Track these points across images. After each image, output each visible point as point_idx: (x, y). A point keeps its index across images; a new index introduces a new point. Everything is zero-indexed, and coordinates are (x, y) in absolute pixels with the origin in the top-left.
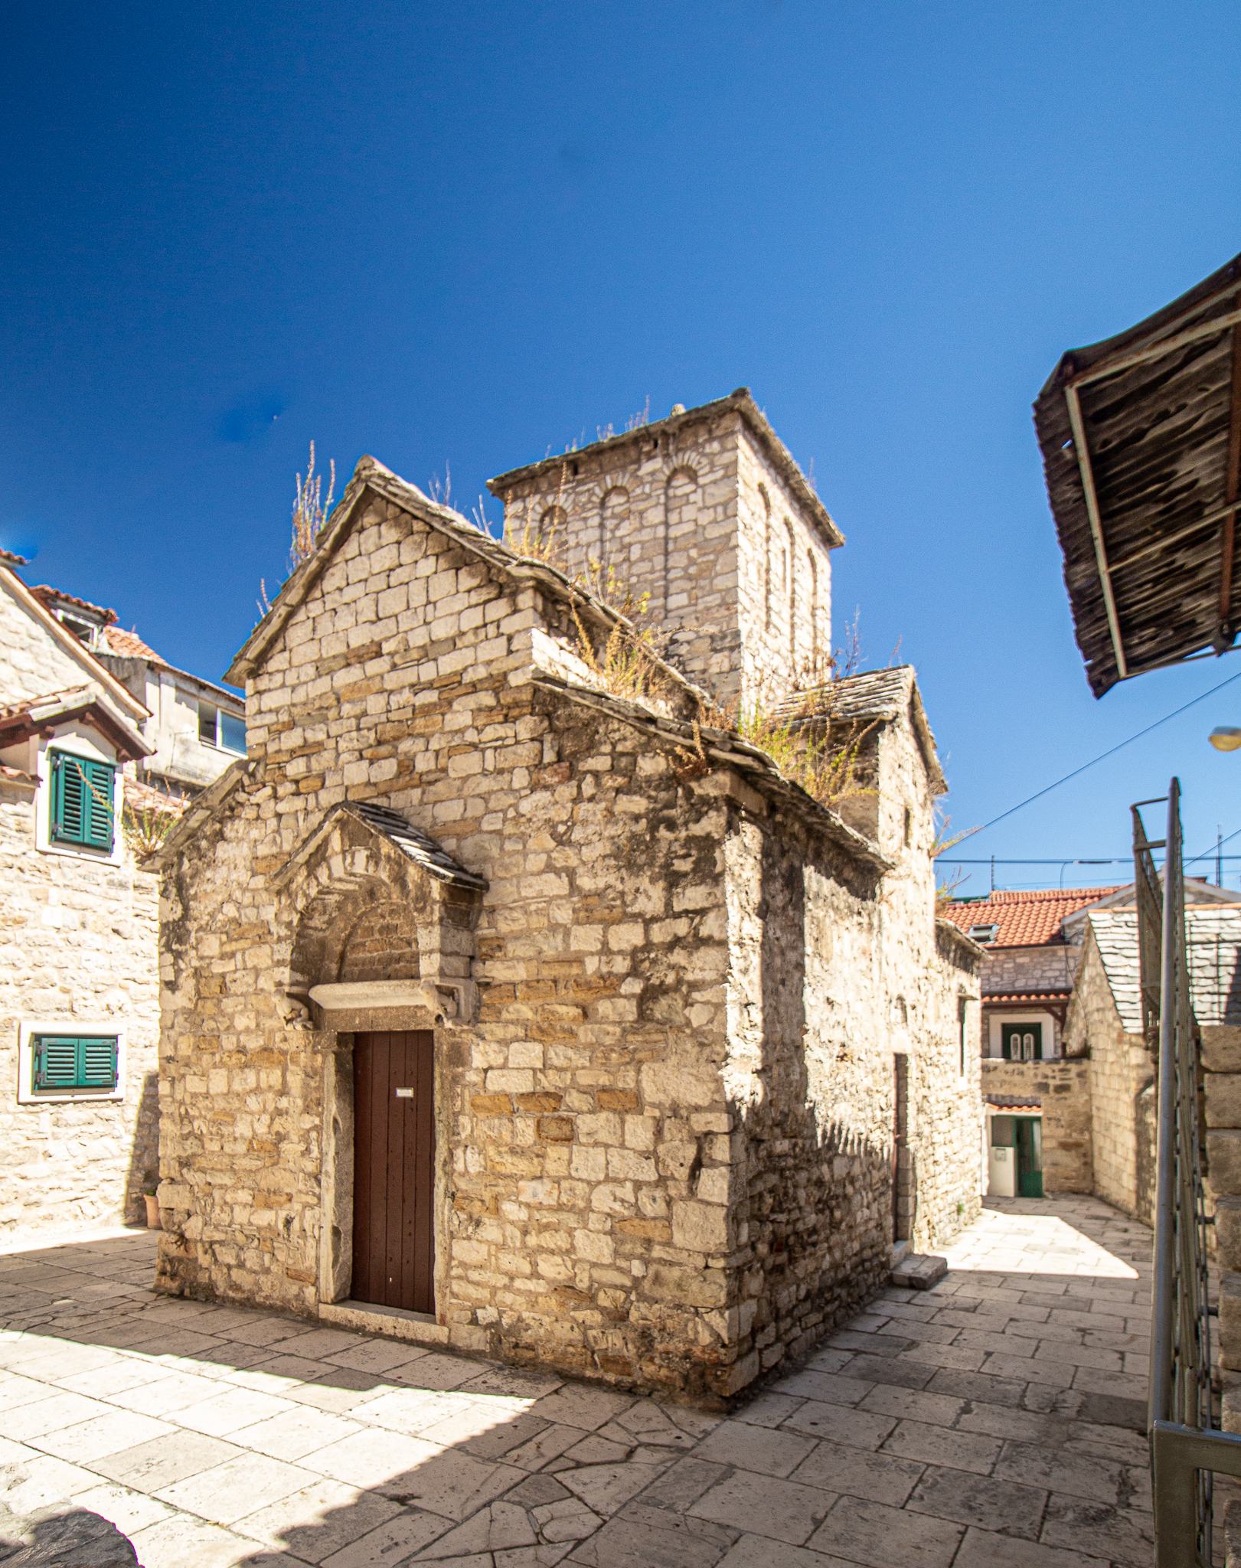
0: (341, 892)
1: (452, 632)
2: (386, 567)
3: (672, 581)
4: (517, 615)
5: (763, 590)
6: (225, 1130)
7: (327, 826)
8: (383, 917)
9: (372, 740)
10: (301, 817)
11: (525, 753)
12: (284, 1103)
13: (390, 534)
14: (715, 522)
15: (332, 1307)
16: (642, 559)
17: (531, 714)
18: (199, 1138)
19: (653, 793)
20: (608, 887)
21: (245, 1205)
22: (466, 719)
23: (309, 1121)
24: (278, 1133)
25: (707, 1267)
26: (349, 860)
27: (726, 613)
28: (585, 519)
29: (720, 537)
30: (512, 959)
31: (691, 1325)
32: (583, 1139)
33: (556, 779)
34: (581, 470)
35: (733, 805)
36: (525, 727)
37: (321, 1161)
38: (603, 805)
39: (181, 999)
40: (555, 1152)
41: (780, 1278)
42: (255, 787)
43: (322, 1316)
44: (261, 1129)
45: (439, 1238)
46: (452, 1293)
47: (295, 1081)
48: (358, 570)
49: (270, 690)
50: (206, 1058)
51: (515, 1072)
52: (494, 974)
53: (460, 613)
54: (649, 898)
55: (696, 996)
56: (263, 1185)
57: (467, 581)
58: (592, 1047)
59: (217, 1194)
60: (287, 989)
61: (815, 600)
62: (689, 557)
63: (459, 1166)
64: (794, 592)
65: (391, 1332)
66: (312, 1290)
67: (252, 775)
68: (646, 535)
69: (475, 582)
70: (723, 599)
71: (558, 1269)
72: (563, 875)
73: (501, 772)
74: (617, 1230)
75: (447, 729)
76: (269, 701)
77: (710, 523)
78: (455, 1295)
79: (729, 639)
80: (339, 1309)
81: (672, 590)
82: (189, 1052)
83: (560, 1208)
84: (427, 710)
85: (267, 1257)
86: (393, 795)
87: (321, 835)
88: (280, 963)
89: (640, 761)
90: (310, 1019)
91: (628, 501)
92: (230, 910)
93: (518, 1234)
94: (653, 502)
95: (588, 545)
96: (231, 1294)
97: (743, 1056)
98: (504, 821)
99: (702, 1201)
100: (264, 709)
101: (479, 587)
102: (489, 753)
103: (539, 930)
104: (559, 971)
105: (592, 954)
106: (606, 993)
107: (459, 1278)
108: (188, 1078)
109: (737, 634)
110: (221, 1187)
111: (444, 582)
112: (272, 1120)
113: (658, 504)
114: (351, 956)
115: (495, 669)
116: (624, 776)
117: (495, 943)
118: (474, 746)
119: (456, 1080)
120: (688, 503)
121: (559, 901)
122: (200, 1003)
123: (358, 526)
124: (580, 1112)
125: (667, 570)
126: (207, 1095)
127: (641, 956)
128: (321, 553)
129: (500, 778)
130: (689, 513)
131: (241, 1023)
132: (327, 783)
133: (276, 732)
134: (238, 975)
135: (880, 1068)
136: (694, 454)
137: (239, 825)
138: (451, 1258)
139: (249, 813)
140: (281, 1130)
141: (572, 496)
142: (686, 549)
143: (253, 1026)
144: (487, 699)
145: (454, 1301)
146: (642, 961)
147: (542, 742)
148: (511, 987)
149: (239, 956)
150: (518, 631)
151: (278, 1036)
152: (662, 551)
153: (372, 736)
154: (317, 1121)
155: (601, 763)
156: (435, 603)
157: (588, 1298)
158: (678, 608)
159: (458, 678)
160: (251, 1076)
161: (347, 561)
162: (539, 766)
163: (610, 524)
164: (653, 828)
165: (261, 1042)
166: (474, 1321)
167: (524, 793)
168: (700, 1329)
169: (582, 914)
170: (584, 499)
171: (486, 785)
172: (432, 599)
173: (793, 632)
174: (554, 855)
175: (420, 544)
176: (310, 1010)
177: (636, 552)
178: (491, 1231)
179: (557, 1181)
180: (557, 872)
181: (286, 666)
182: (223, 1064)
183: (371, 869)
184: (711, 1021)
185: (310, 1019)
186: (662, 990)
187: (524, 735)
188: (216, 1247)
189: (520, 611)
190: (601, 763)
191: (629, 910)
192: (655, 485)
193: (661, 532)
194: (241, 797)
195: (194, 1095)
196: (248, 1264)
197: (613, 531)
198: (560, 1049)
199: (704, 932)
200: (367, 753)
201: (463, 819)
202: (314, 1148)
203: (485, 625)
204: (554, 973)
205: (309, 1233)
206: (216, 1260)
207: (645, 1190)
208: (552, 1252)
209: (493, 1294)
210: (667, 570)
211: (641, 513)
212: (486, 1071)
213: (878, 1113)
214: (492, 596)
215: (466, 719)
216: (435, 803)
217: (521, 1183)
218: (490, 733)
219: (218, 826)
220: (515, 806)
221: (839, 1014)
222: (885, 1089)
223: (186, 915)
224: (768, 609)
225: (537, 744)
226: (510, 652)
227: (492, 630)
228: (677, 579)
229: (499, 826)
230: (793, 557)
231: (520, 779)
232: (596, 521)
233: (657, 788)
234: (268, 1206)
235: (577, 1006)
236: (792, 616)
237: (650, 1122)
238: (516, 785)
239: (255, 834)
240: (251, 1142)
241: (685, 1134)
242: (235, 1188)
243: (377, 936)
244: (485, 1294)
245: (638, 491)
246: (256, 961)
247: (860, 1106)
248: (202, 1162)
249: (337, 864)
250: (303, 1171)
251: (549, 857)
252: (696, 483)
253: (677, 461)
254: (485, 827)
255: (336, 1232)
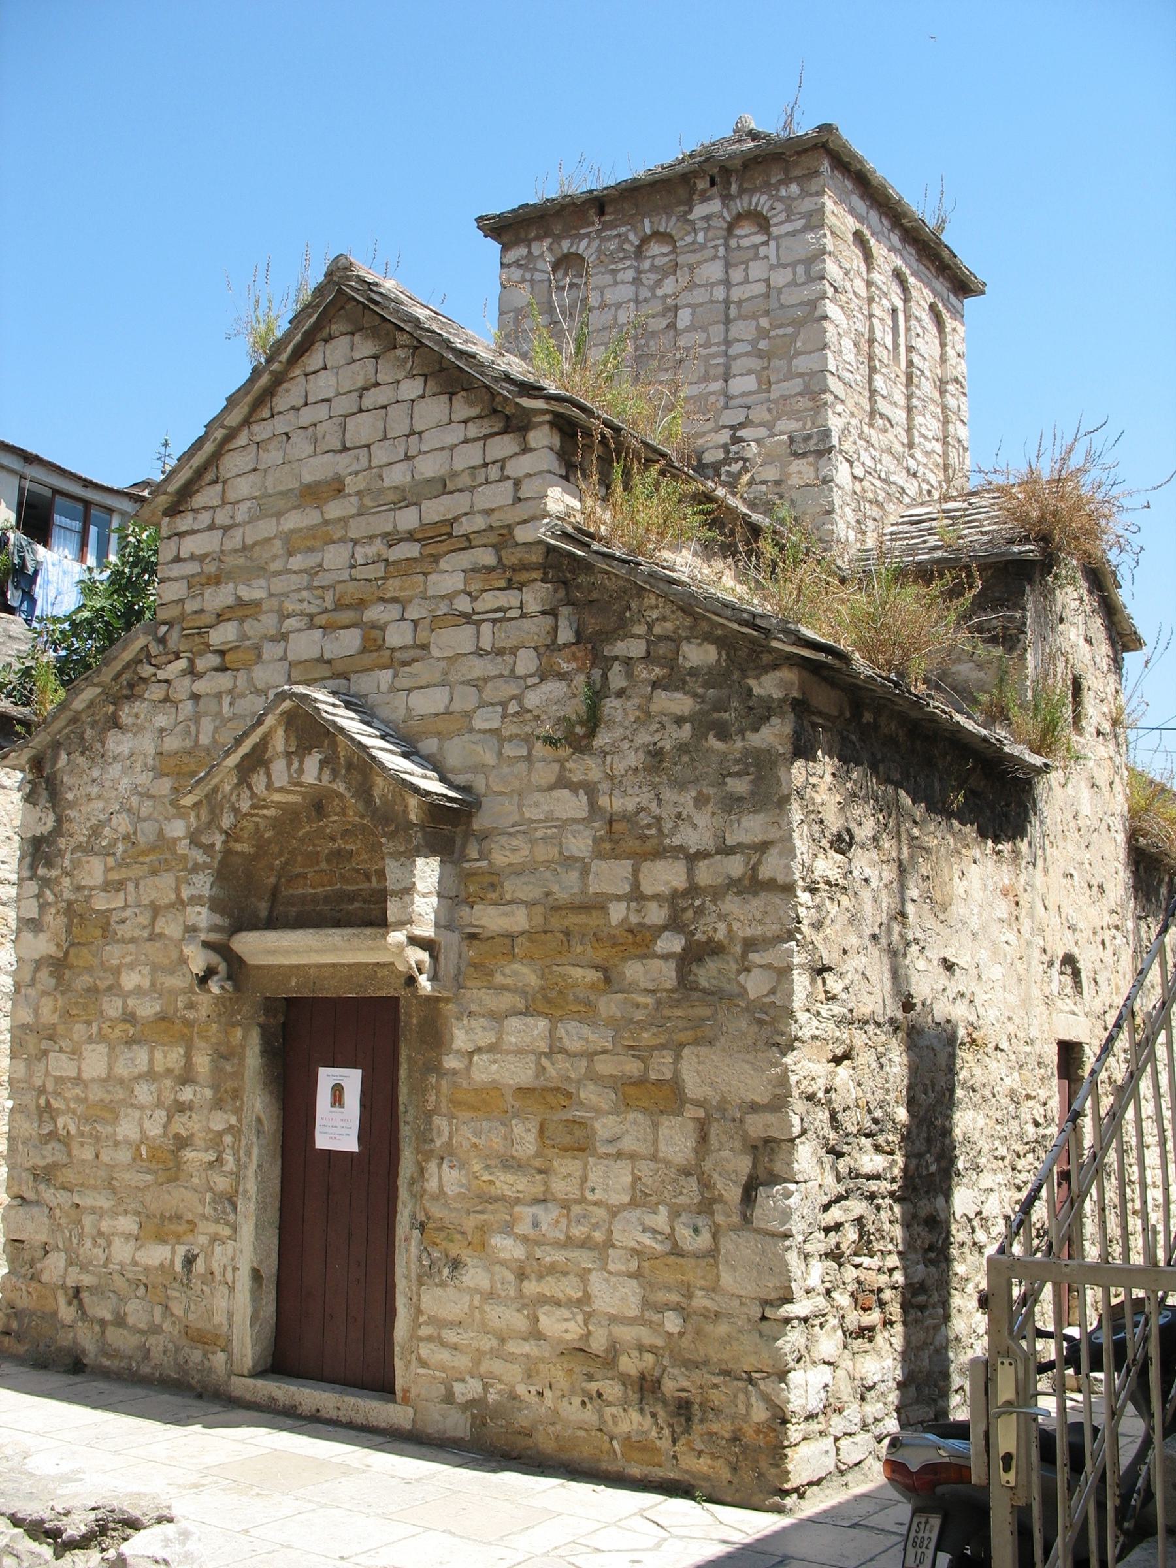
0: (278, 805)
1: (443, 471)
2: (359, 384)
3: (735, 358)
4: (528, 456)
5: (865, 370)
6: (104, 1130)
7: (270, 720)
8: (333, 839)
9: (329, 604)
10: (226, 701)
11: (534, 629)
12: (187, 1094)
13: (366, 347)
14: (794, 283)
15: (250, 1381)
16: (692, 328)
17: (543, 581)
18: (65, 1141)
19: (700, 691)
20: (641, 809)
21: (128, 1237)
22: (454, 582)
23: (219, 1121)
24: (177, 1136)
25: (764, 1318)
26: (296, 765)
27: (811, 404)
28: (614, 272)
29: (802, 304)
30: (510, 902)
31: (741, 1396)
32: (602, 1150)
33: (574, 665)
34: (609, 209)
35: (801, 707)
36: (535, 597)
37: (238, 1176)
38: (636, 701)
39: (42, 945)
40: (567, 1166)
41: (868, 1346)
42: (163, 659)
43: (237, 1393)
44: (154, 1129)
45: (401, 1285)
46: (419, 1359)
47: (202, 1063)
48: (324, 385)
49: (193, 532)
50: (79, 1028)
51: (510, 1058)
52: (484, 922)
53: (452, 448)
54: (695, 826)
55: (754, 957)
56: (154, 1207)
57: (463, 410)
58: (611, 1022)
59: (88, 1221)
60: (203, 936)
61: (944, 370)
62: (758, 327)
63: (432, 1185)
64: (910, 363)
65: (333, 1414)
66: (221, 1357)
67: (162, 641)
68: (700, 296)
69: (474, 412)
70: (807, 386)
71: (565, 1325)
72: (581, 792)
73: (500, 652)
74: (646, 1272)
75: (430, 593)
76: (190, 546)
77: (787, 285)
78: (424, 1364)
79: (814, 441)
80: (259, 1383)
81: (735, 369)
82: (55, 1019)
83: (569, 1242)
84: (404, 568)
85: (158, 1310)
86: (353, 677)
87: (260, 731)
88: (195, 900)
89: (685, 648)
90: (229, 977)
91: (673, 252)
92: (122, 823)
93: (511, 1277)
94: (709, 253)
95: (618, 306)
96: (106, 1362)
97: (814, 1037)
98: (504, 716)
99: (758, 1231)
100: (182, 555)
101: (479, 417)
102: (486, 628)
103: (548, 864)
104: (574, 920)
105: (619, 898)
106: (639, 951)
107: (430, 1339)
108: (51, 1054)
109: (826, 434)
110: (93, 1210)
111: (433, 410)
112: (170, 1118)
113: (715, 257)
114: (286, 892)
115: (496, 520)
116: (663, 666)
117: (487, 879)
118: (467, 617)
119: (434, 1067)
120: (756, 257)
121: (575, 827)
122: (72, 951)
123: (325, 334)
124: (599, 1112)
125: (728, 343)
126: (78, 1080)
127: (683, 903)
128: (275, 366)
129: (499, 659)
130: (757, 270)
131: (130, 980)
132: (265, 657)
133: (198, 584)
134: (128, 913)
135: (1032, 1061)
136: (764, 198)
137: (139, 707)
138: (419, 1312)
139: (155, 692)
140: (184, 1133)
141: (597, 242)
142: (754, 317)
143: (146, 984)
144: (487, 557)
145: (422, 1371)
146: (684, 910)
147: (556, 616)
148: (508, 941)
149: (130, 887)
150: (529, 475)
151: (181, 1002)
152: (722, 318)
153: (329, 596)
154: (233, 1120)
155: (637, 648)
156: (420, 433)
157: (609, 1360)
158: (743, 394)
159: (448, 530)
160: (141, 1056)
161: (306, 375)
162: (552, 647)
163: (649, 279)
164: (699, 734)
165: (158, 1008)
166: (449, 1398)
167: (530, 681)
168: (753, 1400)
169: (607, 846)
170: (613, 246)
171: (480, 668)
172: (418, 427)
173: (910, 419)
174: (569, 765)
175: (405, 360)
176: (229, 965)
177: (684, 318)
178: (475, 1276)
179: (566, 1205)
180: (573, 787)
181: (216, 502)
182: (102, 1038)
183: (326, 777)
184: (773, 992)
185: (229, 977)
186: (714, 949)
187: (533, 607)
188: (84, 1295)
189: (532, 450)
190: (637, 648)
191: (668, 841)
192: (711, 234)
193: (720, 293)
194: (146, 670)
195: (59, 1080)
196: (130, 1320)
197: (652, 289)
198: (573, 1026)
199: (764, 873)
200: (321, 620)
201: (447, 712)
202: (229, 1158)
203: (486, 465)
204: (566, 923)
205: (218, 1277)
206: (84, 1313)
207: (684, 1218)
208: (558, 1304)
209: (477, 1362)
210: (728, 343)
211: (692, 269)
212: (471, 1054)
213: (1030, 1129)
214: (495, 430)
215: (454, 582)
216: (410, 690)
217: (517, 1209)
218: (489, 601)
219: (111, 708)
220: (519, 698)
221: (960, 982)
222: (1043, 1094)
223: (58, 830)
224: (873, 392)
225: (549, 620)
226: (518, 500)
227: (494, 472)
228: (741, 355)
229: (496, 724)
230: (907, 319)
231: (526, 662)
232: (630, 274)
233: (707, 685)
234: (161, 1239)
235: (597, 968)
236: (909, 397)
237: (691, 1126)
238: (520, 670)
239: (161, 721)
240: (138, 1148)
241: (737, 1145)
242: (114, 1214)
243: (324, 865)
244: (462, 1362)
245: (689, 239)
246: (154, 895)
247: (999, 1115)
248: (69, 1176)
249: (280, 770)
250: (211, 1189)
251: (562, 767)
252: (768, 234)
253: (739, 205)
254: (478, 724)
255: (256, 1275)
